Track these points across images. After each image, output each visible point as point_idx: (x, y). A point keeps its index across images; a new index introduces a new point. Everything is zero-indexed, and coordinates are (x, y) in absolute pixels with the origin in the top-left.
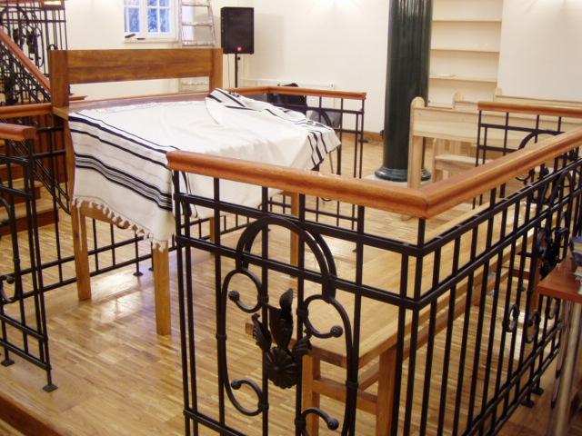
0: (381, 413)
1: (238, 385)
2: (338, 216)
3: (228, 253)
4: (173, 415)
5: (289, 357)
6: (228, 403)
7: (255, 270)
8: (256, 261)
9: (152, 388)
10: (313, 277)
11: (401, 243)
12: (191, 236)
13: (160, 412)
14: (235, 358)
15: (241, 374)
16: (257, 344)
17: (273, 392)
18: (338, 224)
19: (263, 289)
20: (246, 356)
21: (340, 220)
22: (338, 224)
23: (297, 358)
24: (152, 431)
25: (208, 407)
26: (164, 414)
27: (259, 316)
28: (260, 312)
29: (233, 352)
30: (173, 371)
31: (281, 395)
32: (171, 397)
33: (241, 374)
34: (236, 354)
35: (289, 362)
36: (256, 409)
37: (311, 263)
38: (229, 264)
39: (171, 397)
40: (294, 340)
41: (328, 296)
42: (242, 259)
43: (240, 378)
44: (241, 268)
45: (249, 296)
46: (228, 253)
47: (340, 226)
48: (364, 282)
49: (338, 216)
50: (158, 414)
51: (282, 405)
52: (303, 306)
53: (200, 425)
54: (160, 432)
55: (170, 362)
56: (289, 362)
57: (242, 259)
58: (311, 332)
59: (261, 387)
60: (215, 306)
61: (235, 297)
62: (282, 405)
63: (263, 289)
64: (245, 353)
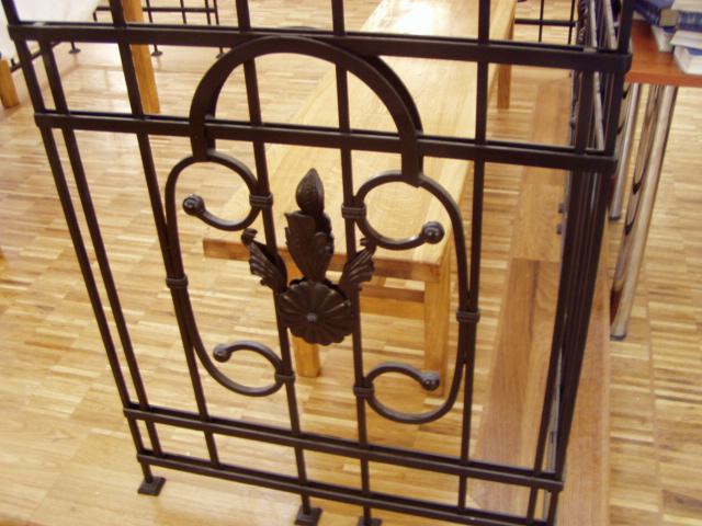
0: (433, 316)
1: (224, 355)
2: (183, 10)
3: (170, 127)
4: (78, 400)
5: (333, 292)
6: (207, 381)
7: (242, 151)
8: (233, 132)
9: (18, 363)
10: (373, 142)
11: (31, 23)
12: (71, 108)
13: (50, 402)
14: (128, 269)
15: (150, 294)
16: (253, 271)
17: (201, 310)
18: (185, 21)
19: (260, 191)
20: (142, 263)
21: (187, 14)
22: (185, 21)
23: (348, 291)
24: (57, 440)
25: (169, 389)
26: (58, 402)
27: (255, 232)
28: (258, 224)
29: (118, 261)
30: (40, 321)
31: (228, 313)
32: (56, 368)
33: (150, 294)
34: (125, 262)
35: (336, 300)
36: (272, 382)
37: (370, 113)
38: (171, 150)
39: (56, 368)
40: (340, 256)
41: (411, 173)
42: (202, 129)
43: (226, 340)
44: (203, 153)
45: (232, 201)
46: (170, 127)
47: (222, 24)
48: (354, 124)
49: (183, 10)
50: (52, 407)
51: (237, 328)
52: (354, 207)
53: (159, 427)
54: (71, 438)
55: (25, 308)
56: (336, 300)
57: (202, 129)
58: (373, 240)
59: (278, 351)
60: (56, 192)
61: (197, 209)
62: (237, 328)
63: (260, 191)
64: (138, 258)
